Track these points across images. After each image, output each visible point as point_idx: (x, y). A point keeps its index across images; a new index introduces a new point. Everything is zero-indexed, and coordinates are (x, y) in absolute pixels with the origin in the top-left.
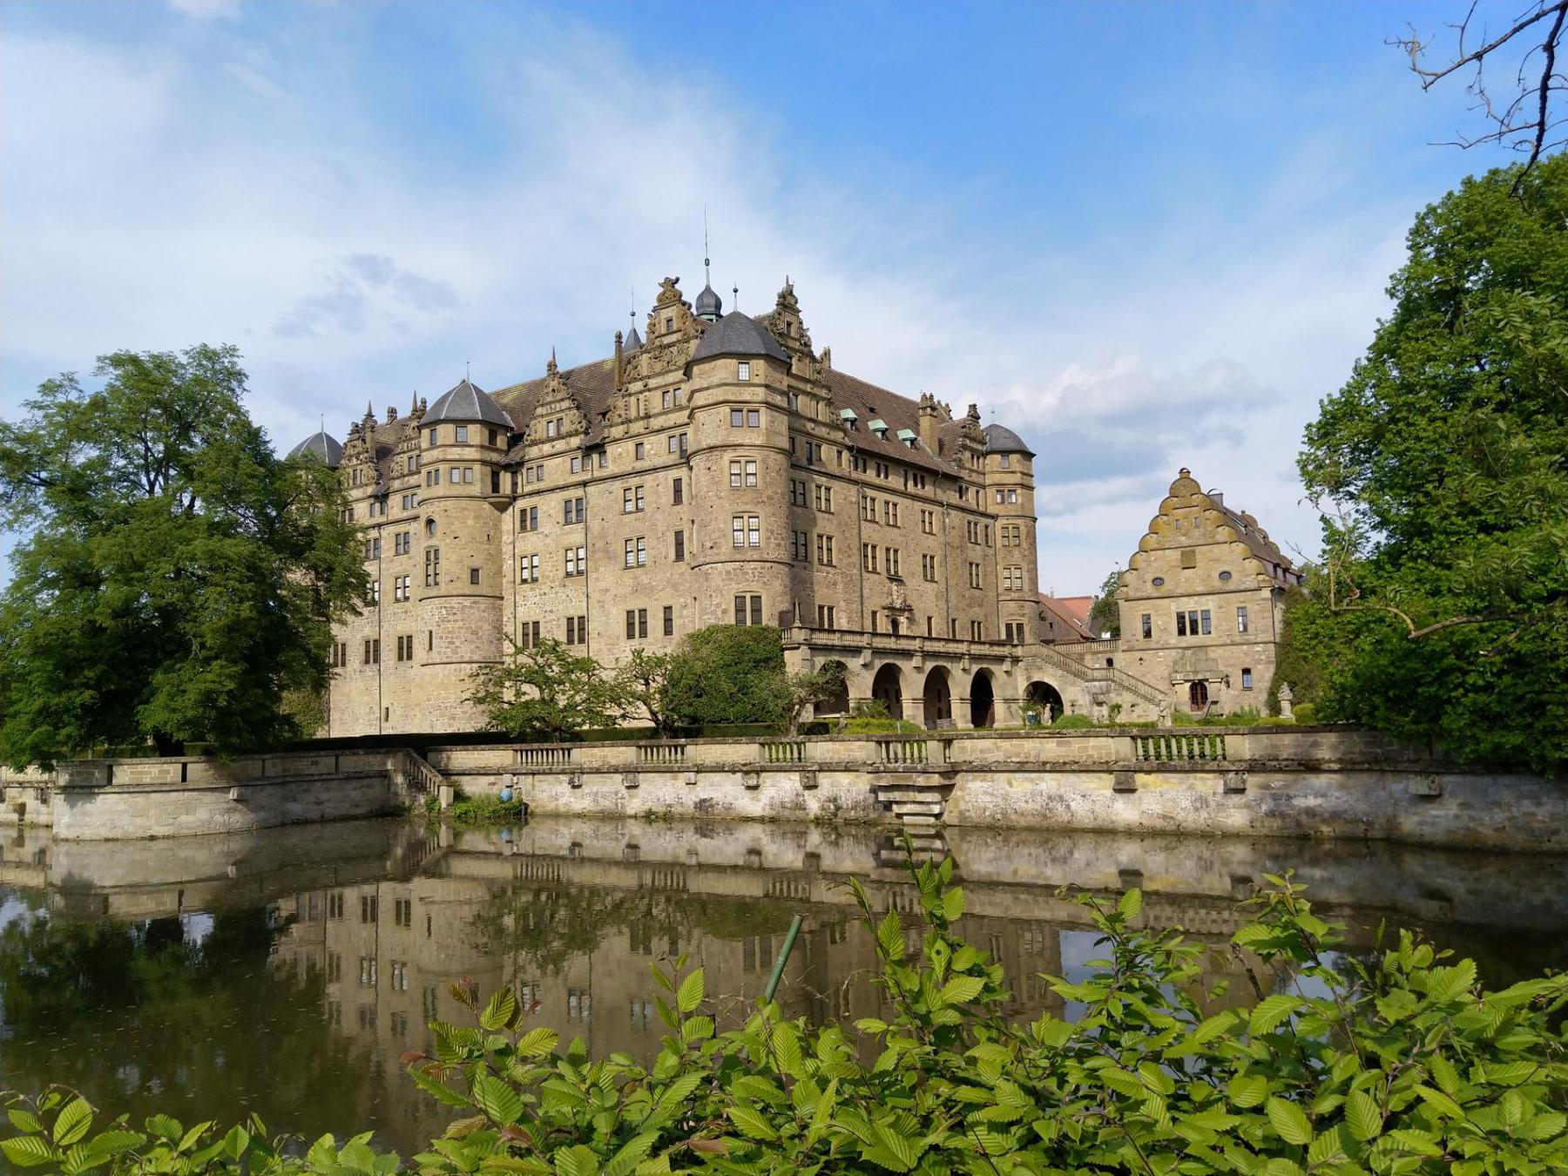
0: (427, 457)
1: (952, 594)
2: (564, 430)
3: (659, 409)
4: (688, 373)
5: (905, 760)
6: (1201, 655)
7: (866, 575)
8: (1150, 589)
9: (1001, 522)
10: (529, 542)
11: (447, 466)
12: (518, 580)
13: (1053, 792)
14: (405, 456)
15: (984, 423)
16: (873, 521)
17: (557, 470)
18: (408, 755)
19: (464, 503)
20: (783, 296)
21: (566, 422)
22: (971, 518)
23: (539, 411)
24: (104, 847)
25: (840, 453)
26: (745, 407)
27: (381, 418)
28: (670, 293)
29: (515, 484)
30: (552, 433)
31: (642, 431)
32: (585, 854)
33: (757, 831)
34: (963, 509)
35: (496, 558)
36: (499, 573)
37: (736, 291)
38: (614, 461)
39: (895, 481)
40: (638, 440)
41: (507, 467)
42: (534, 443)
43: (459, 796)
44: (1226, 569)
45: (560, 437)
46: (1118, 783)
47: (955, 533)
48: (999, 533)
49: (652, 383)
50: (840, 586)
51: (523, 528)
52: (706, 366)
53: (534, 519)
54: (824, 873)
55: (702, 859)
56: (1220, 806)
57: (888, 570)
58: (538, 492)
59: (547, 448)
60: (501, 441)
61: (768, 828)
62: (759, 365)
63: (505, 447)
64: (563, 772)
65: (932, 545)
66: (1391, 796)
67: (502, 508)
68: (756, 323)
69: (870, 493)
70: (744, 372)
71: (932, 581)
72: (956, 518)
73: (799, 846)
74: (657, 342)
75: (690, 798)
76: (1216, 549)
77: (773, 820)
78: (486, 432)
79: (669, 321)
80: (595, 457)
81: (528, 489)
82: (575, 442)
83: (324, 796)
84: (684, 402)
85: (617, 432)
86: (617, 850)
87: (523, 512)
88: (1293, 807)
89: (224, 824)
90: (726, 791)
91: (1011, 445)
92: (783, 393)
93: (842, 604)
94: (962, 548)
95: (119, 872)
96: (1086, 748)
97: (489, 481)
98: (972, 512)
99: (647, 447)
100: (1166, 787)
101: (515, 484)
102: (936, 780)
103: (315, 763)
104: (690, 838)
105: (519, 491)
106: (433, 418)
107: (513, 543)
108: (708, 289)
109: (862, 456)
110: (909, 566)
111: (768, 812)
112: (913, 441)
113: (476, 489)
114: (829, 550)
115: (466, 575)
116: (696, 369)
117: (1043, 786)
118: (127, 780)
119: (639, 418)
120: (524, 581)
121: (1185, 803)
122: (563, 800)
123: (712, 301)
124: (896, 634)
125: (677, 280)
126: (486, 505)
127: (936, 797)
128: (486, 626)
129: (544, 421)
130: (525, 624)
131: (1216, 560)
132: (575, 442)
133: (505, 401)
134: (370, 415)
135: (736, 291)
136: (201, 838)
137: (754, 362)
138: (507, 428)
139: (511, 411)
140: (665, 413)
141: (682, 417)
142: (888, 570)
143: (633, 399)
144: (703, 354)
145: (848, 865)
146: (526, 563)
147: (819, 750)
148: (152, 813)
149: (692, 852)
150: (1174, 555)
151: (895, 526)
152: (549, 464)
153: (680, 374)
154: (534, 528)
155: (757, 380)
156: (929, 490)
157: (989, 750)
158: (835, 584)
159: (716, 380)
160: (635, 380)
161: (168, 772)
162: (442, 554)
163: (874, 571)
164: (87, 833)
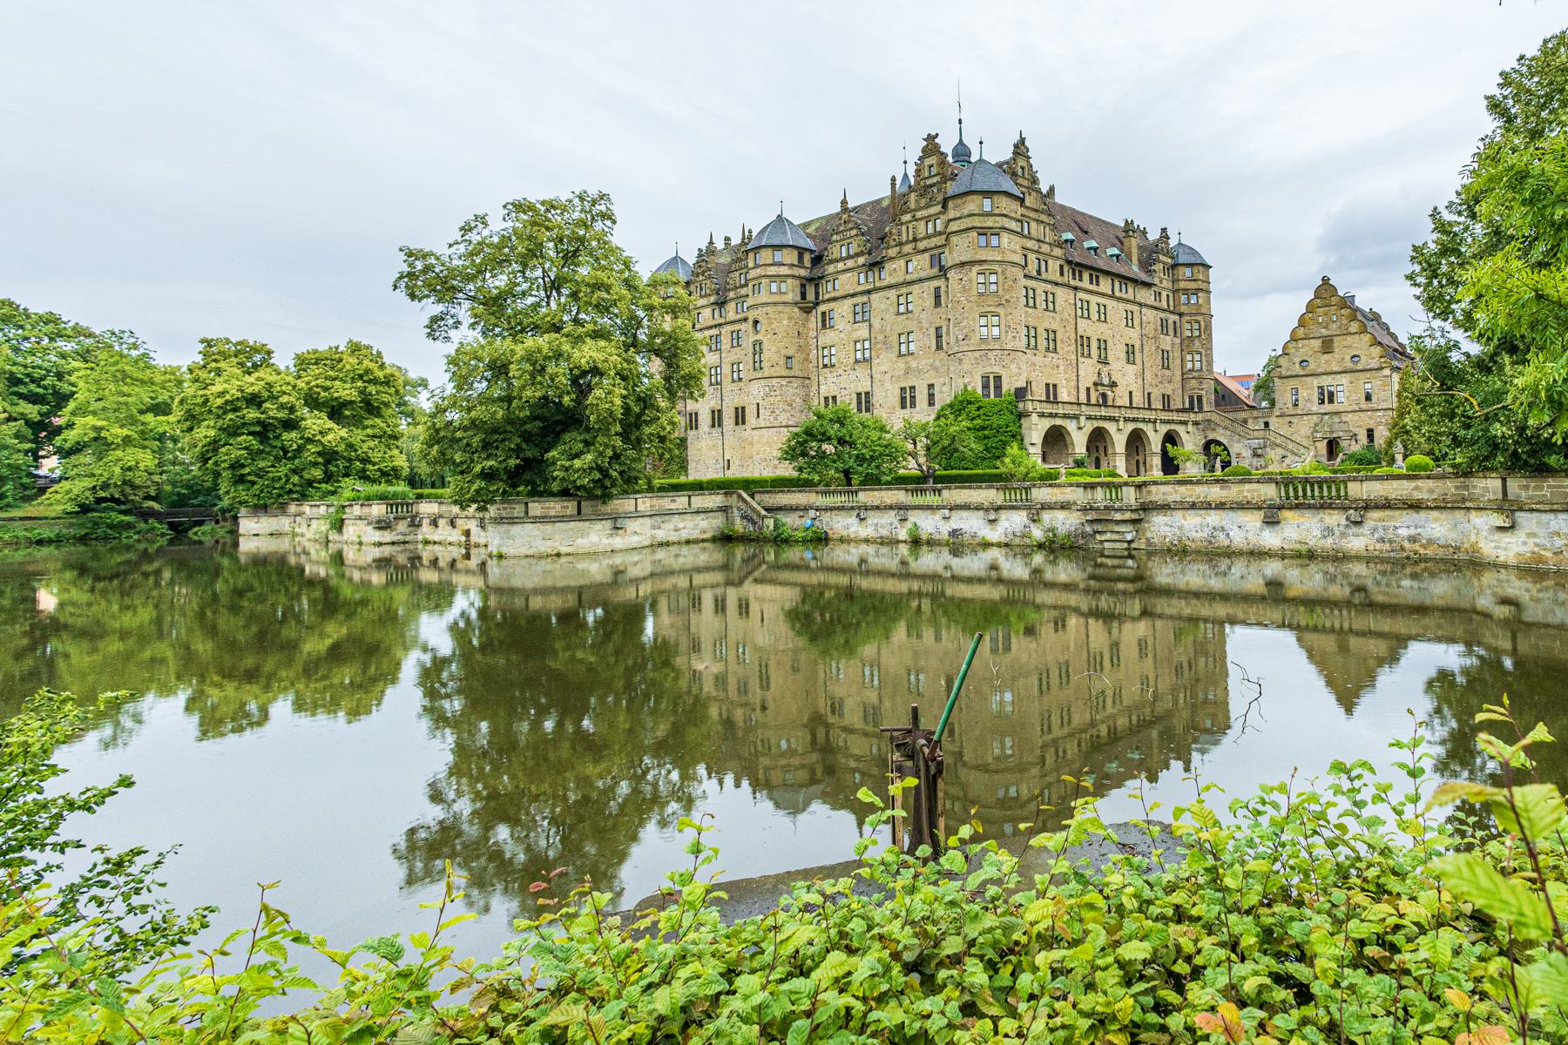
6: (1336, 419)
8: (1297, 369)
10: (828, 337)
15: (1173, 242)
19: (780, 308)
22: (1163, 315)
24: (524, 561)
29: (817, 293)
36: (807, 359)
39: (1105, 285)
42: (831, 262)
45: (849, 257)
47: (1151, 327)
49: (919, 214)
51: (824, 326)
58: (834, 299)
59: (840, 266)
60: (807, 257)
61: (1003, 551)
65: (1133, 336)
67: (807, 311)
69: (1081, 295)
77: (1006, 545)
78: (796, 253)
80: (876, 270)
83: (681, 525)
85: (892, 252)
86: (893, 565)
87: (824, 314)
90: (972, 524)
95: (536, 579)
97: (798, 291)
101: (817, 293)
109: (1077, 267)
110: (1117, 353)
111: (1003, 539)
113: (789, 298)
115: (782, 361)
116: (951, 204)
118: (538, 513)
119: (908, 242)
120: (825, 366)
127: (1129, 528)
132: (861, 260)
138: (811, 251)
145: (1063, 577)
146: (826, 352)
150: (1317, 344)
153: (939, 208)
159: (966, 212)
160: (905, 212)
162: (765, 346)
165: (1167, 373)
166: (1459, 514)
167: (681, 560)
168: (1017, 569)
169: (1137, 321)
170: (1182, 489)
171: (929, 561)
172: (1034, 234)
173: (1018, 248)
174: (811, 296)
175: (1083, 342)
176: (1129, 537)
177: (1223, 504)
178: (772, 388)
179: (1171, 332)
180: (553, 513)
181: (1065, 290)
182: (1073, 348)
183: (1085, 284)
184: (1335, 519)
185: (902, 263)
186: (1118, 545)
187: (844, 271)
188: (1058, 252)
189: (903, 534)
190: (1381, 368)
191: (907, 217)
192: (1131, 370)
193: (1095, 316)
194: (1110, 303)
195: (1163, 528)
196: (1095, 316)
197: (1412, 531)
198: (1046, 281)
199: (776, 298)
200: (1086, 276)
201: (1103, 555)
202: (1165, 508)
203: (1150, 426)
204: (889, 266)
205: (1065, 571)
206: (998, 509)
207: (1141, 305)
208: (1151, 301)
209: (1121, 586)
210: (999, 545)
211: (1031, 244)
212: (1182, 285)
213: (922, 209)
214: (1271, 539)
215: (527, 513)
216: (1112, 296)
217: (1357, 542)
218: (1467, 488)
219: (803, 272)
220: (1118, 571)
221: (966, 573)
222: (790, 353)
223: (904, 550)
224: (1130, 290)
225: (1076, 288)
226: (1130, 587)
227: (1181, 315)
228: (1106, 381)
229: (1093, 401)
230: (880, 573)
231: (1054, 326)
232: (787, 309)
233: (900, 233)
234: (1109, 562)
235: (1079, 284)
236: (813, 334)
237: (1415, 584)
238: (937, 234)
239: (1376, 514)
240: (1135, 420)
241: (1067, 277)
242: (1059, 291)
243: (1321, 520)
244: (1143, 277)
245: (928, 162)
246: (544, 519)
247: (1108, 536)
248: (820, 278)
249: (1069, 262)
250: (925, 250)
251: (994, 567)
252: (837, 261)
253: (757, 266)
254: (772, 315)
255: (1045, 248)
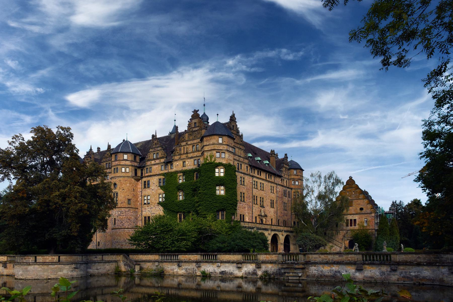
0: (114, 164)
1: (279, 212)
2: (158, 157)
3: (191, 151)
4: (202, 140)
5: (291, 260)
7: (254, 205)
9: (293, 191)
10: (147, 191)
11: (121, 167)
12: (143, 203)
13: (337, 270)
14: (105, 163)
15: (289, 160)
16: (257, 188)
17: (156, 169)
18: (124, 256)
19: (126, 179)
20: (231, 117)
21: (160, 154)
22: (284, 189)
23: (151, 150)
25: (247, 167)
26: (221, 151)
27: (95, 151)
28: (124, 140)
29: (142, 173)
30: (155, 157)
31: (185, 158)
32: (182, 286)
33: (240, 281)
34: (283, 186)
35: (135, 196)
36: (137, 201)
37: (218, 115)
38: (176, 167)
39: (263, 176)
40: (184, 161)
41: (139, 167)
42: (149, 160)
43: (141, 269)
44: (362, 207)
45: (157, 159)
46: (357, 268)
47: (280, 193)
48: (293, 194)
49: (189, 143)
50: (246, 208)
51: (145, 187)
52: (208, 138)
53: (148, 184)
54: (262, 293)
55: (222, 289)
56: (388, 274)
57: (261, 204)
58: (150, 176)
59: (153, 162)
60: (138, 158)
62: (225, 138)
63: (139, 161)
64: (176, 262)
65: (273, 196)
66: (442, 273)
67: (138, 180)
68: (224, 125)
69: (255, 179)
70: (220, 141)
71: (273, 208)
72: (280, 188)
73: (254, 286)
74: (191, 130)
75: (218, 270)
76: (359, 201)
77: (246, 278)
78: (133, 156)
79: (195, 123)
80: (169, 165)
81: (147, 175)
82: (162, 160)
83: (99, 268)
84: (200, 149)
85: (176, 158)
86: (194, 285)
87: (145, 182)
88: (411, 275)
89: (71, 275)
90: (230, 268)
91: (297, 167)
92: (232, 147)
93: (247, 214)
94: (282, 198)
96: (348, 258)
97: (134, 172)
98: (285, 187)
99: (187, 163)
100: (372, 269)
101: (142, 173)
102: (301, 266)
103: (96, 257)
104: (218, 283)
105: (144, 175)
106: (116, 151)
107: (141, 192)
108: (204, 113)
109: (253, 167)
110: (267, 203)
112: (268, 164)
113: (130, 174)
114: (244, 197)
115: (126, 201)
116: (205, 139)
117: (334, 268)
118: (41, 261)
119: (184, 154)
120: (145, 204)
121: (378, 274)
122: (175, 270)
123: (206, 118)
124: (262, 223)
125: (198, 110)
126: (133, 180)
127: (301, 271)
128: (133, 217)
129: (152, 154)
130: (145, 217)
131: (359, 204)
132: (162, 160)
133: (138, 147)
134: (91, 149)
135: (218, 115)
136: (64, 281)
137: (224, 137)
138: (140, 155)
139: (140, 150)
140: (193, 152)
141: (199, 154)
142: (261, 204)
143: (182, 148)
144: (207, 134)
145: (270, 291)
146: (146, 198)
147: (262, 257)
148: (49, 271)
149: (219, 286)
151: (263, 190)
152: (154, 167)
153: (199, 140)
154: (149, 187)
155: (224, 143)
156: (273, 179)
157: (317, 258)
158: (245, 208)
159: (211, 143)
160: (183, 141)
161: (54, 259)
162: (119, 195)
163: (257, 204)
164: (29, 277)
165: (286, 212)
166: (435, 268)
167: (99, 282)
168: (250, 288)
169: (275, 191)
170: (323, 256)
171: (209, 284)
172: (237, 153)
173: (232, 159)
174: (139, 174)
175: (254, 198)
176: (300, 275)
177: (410, 262)
178: (122, 212)
179: (287, 196)
180: (48, 261)
181: (249, 177)
182: (251, 200)
183: (256, 175)
184: (385, 269)
185: (181, 162)
186: (295, 278)
187: (155, 164)
188: (246, 161)
189: (199, 273)
190: (371, 213)
191: (184, 144)
192: (272, 210)
193: (259, 188)
194: (265, 183)
195: (314, 271)
196: (259, 188)
197: (416, 274)
198: (241, 173)
199: (124, 175)
200: (256, 171)
201: (288, 282)
202: (315, 264)
203: (280, 233)
204: (175, 164)
205: (271, 289)
206: (200, 262)
207: (276, 184)
208: (280, 182)
209: (297, 294)
210: (242, 277)
211: (236, 157)
212: (292, 177)
213: (190, 140)
214: (359, 275)
215: (36, 260)
216: (266, 180)
217: (394, 278)
218: (438, 258)
219: (136, 164)
220: (296, 288)
221: (227, 289)
222: (130, 198)
223: (199, 279)
224: (273, 178)
225: (253, 176)
226: (301, 295)
227: (291, 189)
228: (263, 214)
229: (258, 222)
230: (186, 289)
231: (244, 191)
232: (129, 179)
233: (180, 150)
234: (291, 285)
235: (254, 175)
236: (139, 190)
237: (417, 294)
238: (197, 151)
239: (402, 267)
240: (275, 230)
241: (249, 172)
242: (247, 178)
243: (380, 269)
244: (278, 173)
245: (194, 121)
246: (44, 263)
247: (291, 274)
248: (144, 167)
249: (250, 166)
250: (192, 158)
251: (239, 287)
252: (152, 160)
253: (116, 160)
254: (122, 182)
255: (241, 159)
